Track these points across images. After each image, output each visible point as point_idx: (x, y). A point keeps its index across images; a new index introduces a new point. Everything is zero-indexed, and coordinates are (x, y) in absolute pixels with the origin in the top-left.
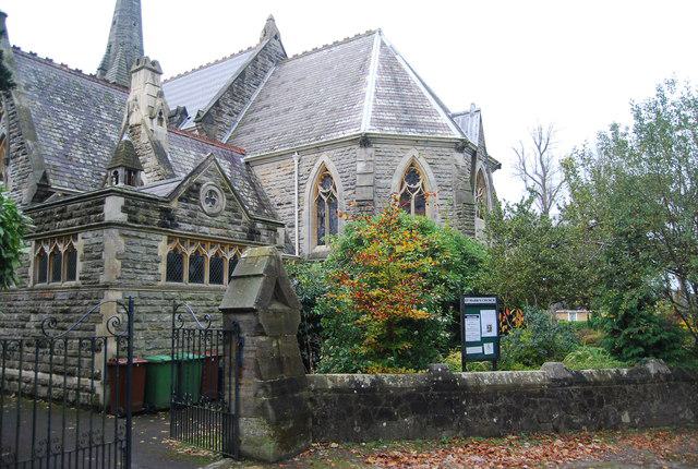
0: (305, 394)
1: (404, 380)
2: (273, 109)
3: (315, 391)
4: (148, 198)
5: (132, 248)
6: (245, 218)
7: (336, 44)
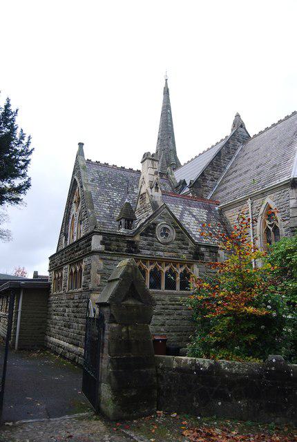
0: (152, 370)
1: (239, 367)
2: (238, 173)
3: (162, 369)
4: (120, 235)
5: (108, 267)
6: (191, 245)
7: (280, 121)
